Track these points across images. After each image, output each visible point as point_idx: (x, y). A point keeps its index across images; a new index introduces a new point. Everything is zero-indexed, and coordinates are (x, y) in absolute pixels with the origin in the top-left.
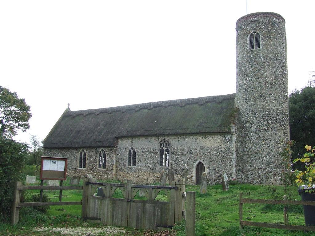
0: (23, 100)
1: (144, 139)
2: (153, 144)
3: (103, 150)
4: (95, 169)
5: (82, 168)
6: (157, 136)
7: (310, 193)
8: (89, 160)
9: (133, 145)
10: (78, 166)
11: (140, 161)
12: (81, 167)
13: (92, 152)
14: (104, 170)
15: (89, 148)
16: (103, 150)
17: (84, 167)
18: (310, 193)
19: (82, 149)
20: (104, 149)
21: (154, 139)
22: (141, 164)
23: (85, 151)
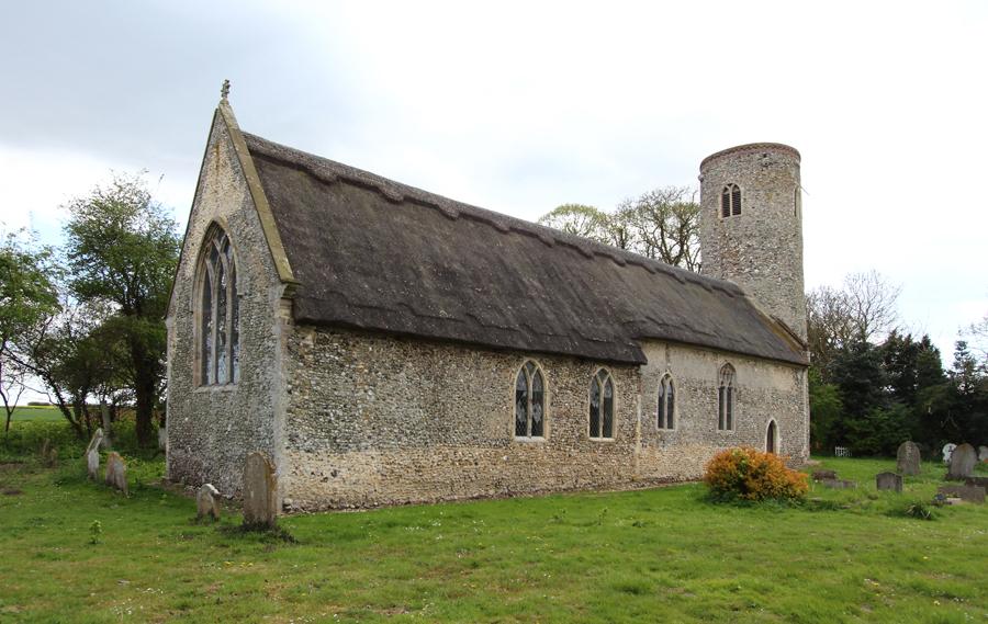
0: (926, 341)
1: (691, 355)
2: (705, 369)
3: (606, 373)
4: (581, 437)
5: (529, 439)
6: (717, 350)
7: (908, 443)
8: (559, 404)
9: (669, 368)
10: (512, 427)
11: (683, 416)
12: (594, 433)
13: (566, 374)
14: (610, 444)
15: (556, 357)
16: (606, 373)
17: (607, 433)
18: (908, 443)
19: (526, 360)
20: (607, 369)
21: (709, 357)
22: (688, 424)
23: (539, 366)
